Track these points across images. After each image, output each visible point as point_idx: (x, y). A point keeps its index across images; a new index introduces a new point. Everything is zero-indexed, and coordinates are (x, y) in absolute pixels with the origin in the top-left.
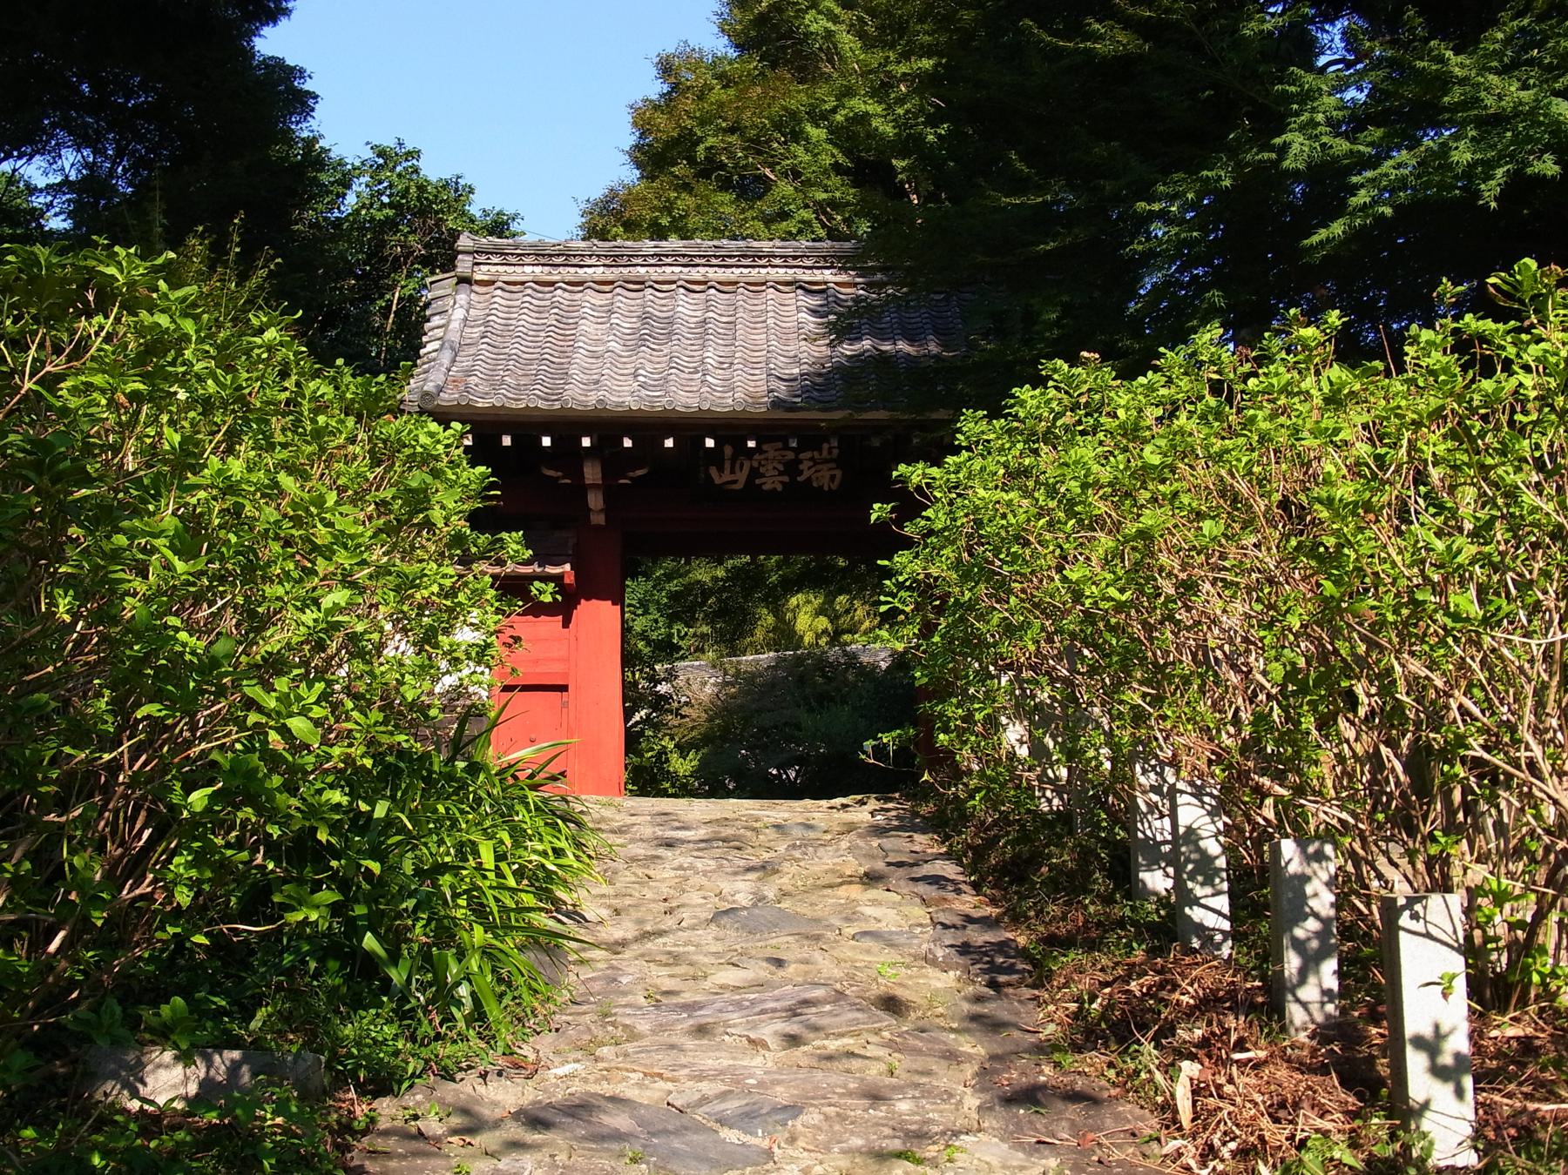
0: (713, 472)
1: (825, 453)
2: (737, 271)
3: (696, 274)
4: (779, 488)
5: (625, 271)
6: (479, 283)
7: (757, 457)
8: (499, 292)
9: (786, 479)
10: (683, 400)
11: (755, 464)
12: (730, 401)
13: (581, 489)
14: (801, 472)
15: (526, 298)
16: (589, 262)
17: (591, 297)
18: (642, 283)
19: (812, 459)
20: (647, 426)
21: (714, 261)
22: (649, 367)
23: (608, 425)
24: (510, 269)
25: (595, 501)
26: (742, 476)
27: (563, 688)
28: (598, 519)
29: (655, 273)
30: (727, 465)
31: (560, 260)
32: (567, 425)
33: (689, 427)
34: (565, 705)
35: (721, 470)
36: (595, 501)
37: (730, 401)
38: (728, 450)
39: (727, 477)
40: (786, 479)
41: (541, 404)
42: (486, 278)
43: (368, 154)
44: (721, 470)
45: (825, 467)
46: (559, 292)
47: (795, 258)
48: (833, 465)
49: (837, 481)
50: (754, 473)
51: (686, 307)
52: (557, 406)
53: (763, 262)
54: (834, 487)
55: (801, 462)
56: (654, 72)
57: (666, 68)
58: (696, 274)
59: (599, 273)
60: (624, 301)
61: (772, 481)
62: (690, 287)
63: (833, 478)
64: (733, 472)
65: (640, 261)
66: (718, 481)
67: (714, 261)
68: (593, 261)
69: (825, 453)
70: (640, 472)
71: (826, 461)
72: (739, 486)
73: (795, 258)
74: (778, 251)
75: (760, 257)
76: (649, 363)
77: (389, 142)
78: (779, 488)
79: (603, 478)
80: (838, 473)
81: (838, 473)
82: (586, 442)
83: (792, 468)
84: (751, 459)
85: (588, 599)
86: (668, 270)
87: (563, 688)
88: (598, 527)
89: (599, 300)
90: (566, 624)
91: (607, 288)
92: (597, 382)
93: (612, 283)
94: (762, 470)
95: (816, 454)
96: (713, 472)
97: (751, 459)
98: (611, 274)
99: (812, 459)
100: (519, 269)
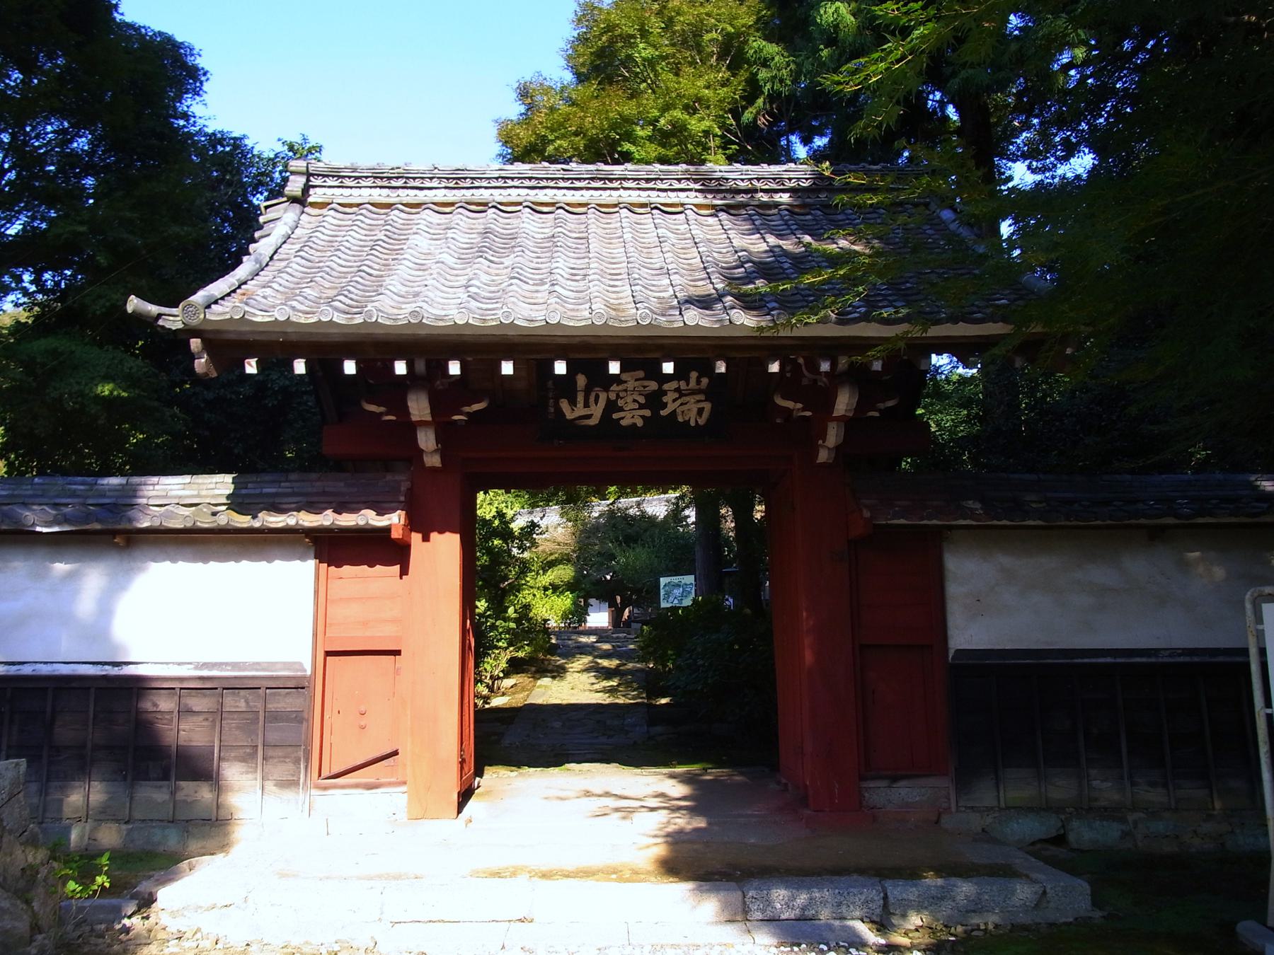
0: (564, 404)
1: (693, 383)
2: (587, 194)
3: (542, 196)
4: (640, 423)
5: (468, 193)
6: (313, 205)
7: (614, 387)
8: (332, 212)
9: (647, 413)
10: (526, 314)
11: (613, 396)
12: (586, 314)
13: (411, 428)
14: (665, 406)
15: (366, 218)
16: (428, 184)
17: (428, 216)
18: (485, 204)
19: (677, 390)
20: (480, 348)
21: (562, 184)
22: (484, 278)
23: (428, 347)
24: (346, 192)
25: (427, 440)
26: (597, 411)
27: (397, 653)
28: (433, 461)
29: (499, 196)
30: (580, 398)
31: (400, 183)
32: (376, 347)
33: (534, 348)
34: (397, 672)
35: (573, 403)
36: (427, 440)
37: (586, 314)
38: (581, 380)
39: (580, 411)
40: (647, 413)
41: (339, 319)
42: (320, 200)
43: (280, 148)
44: (573, 403)
45: (692, 399)
46: (396, 212)
47: (648, 180)
48: (702, 397)
49: (705, 415)
50: (611, 407)
51: (529, 224)
52: (359, 320)
53: (616, 185)
54: (701, 422)
55: (665, 393)
56: (514, 95)
57: (524, 93)
58: (542, 196)
59: (440, 195)
60: (461, 219)
61: (631, 416)
62: (536, 208)
63: (700, 411)
64: (586, 405)
65: (485, 184)
66: (570, 415)
67: (562, 184)
68: (435, 183)
69: (693, 383)
70: (890, 404)
71: (693, 392)
72: (593, 422)
73: (648, 180)
74: (629, 175)
75: (611, 180)
76: (483, 274)
77: (296, 138)
78: (640, 423)
79: (432, 413)
80: (707, 406)
81: (707, 406)
82: (400, 368)
83: (654, 401)
84: (607, 390)
85: (441, 532)
86: (514, 192)
87: (397, 653)
88: (433, 469)
89: (436, 218)
90: (404, 572)
91: (448, 210)
92: (416, 295)
93: (452, 204)
94: (620, 403)
95: (683, 384)
96: (564, 404)
97: (607, 390)
98: (451, 196)
99: (677, 390)
100: (355, 192)
